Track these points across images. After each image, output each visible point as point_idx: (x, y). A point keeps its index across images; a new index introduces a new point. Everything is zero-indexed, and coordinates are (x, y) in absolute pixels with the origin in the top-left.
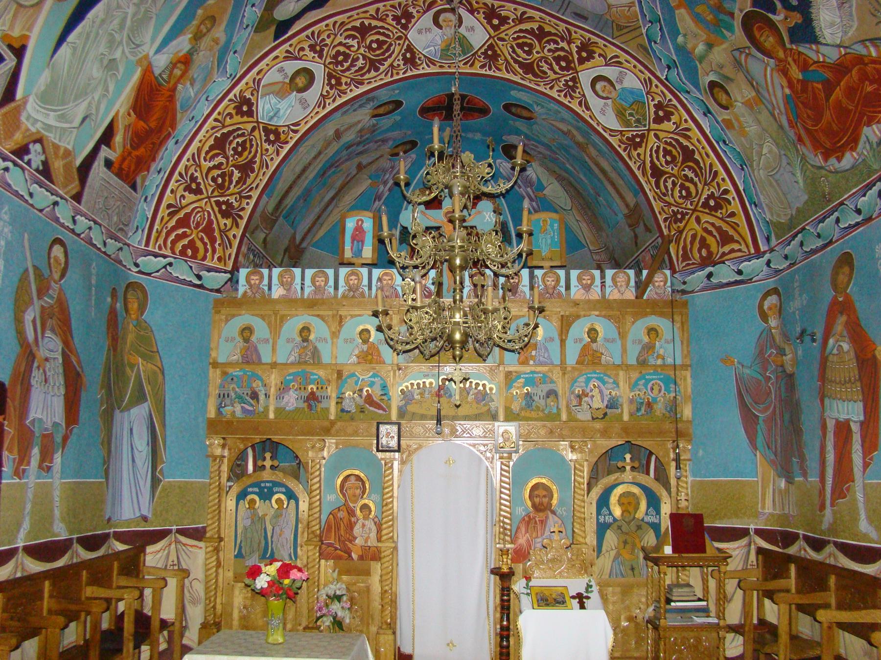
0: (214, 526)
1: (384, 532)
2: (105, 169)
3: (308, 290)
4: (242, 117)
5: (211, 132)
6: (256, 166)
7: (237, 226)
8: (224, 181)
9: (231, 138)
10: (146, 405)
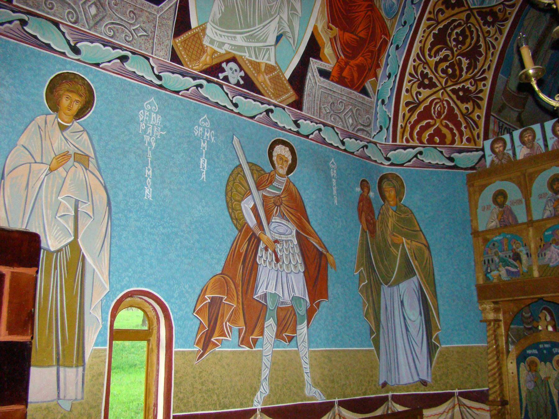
0: (495, 389)
2: (322, 79)
3: (550, 143)
4: (453, 9)
5: (428, 31)
6: (482, 50)
7: (479, 107)
8: (454, 71)
9: (449, 31)
10: (414, 279)
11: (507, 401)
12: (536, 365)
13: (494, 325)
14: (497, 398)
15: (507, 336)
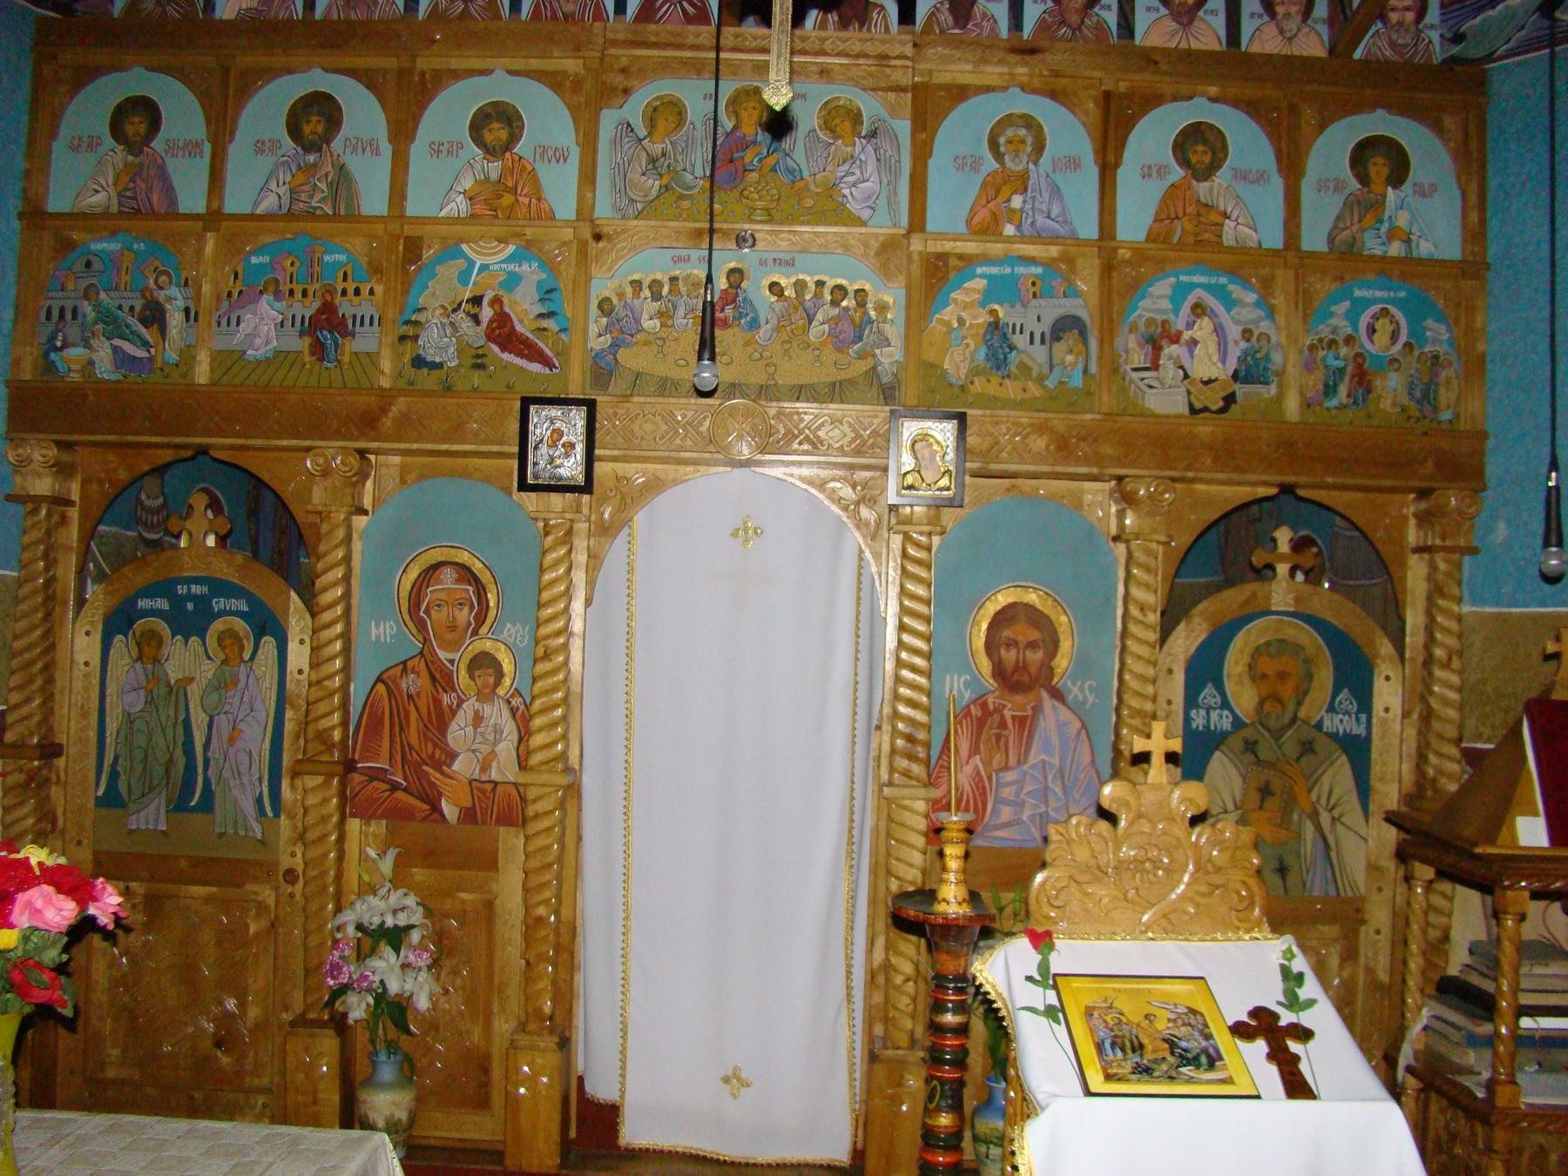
0: (25, 710)
1: (538, 740)
11: (61, 746)
12: (160, 642)
13: (49, 514)
14: (32, 734)
15: (85, 555)
